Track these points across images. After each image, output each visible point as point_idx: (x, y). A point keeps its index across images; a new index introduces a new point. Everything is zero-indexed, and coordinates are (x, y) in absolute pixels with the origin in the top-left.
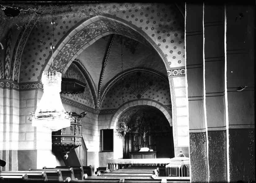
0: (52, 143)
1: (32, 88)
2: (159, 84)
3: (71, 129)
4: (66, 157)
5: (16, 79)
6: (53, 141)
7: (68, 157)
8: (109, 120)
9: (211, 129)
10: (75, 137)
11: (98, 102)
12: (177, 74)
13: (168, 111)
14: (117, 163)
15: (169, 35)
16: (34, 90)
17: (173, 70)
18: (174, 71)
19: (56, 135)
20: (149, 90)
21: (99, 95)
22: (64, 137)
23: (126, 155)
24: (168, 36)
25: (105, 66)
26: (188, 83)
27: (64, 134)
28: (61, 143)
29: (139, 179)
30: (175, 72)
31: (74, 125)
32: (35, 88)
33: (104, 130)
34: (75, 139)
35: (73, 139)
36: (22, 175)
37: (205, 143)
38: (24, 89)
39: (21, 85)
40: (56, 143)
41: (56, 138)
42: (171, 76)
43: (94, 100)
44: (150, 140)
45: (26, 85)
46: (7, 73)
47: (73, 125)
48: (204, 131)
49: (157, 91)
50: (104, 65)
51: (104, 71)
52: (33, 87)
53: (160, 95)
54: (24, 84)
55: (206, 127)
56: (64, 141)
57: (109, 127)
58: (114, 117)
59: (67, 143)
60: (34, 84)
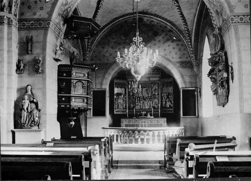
0: (58, 105)
1: (39, 27)
2: (166, 35)
3: (83, 86)
5: (15, 13)
6: (59, 102)
7: (74, 125)
8: (101, 77)
11: (87, 54)
12: (243, 21)
13: (177, 69)
16: (42, 29)
17: (238, 16)
18: (240, 17)
19: (63, 94)
20: (154, 42)
21: (89, 44)
22: (74, 98)
25: (100, 7)
27: (83, 94)
28: (70, 105)
29: (27, 150)
30: (241, 18)
31: (87, 82)
32: (43, 27)
38: (42, 26)
39: (21, 22)
40: (63, 105)
41: (64, 99)
42: (235, 23)
43: (82, 49)
45: (30, 21)
46: (5, 3)
47: (85, 81)
49: (164, 43)
50: (100, 6)
51: (98, 13)
52: (24, 26)
53: (167, 48)
54: (26, 20)
57: (101, 86)
58: (107, 74)
59: (79, 106)
60: (25, 23)
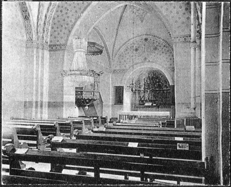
4: (86, 109)
9: (224, 91)
10: (94, 92)
14: (127, 115)
15: (186, 9)
18: (178, 38)
23: (134, 107)
24: (186, 8)
26: (2, 6)
28: (82, 97)
33: (116, 86)
34: (94, 94)
35: (93, 94)
36: (53, 123)
37: (218, 102)
44: (219, 165)
48: (217, 92)
55: (221, 89)
56: (85, 96)
